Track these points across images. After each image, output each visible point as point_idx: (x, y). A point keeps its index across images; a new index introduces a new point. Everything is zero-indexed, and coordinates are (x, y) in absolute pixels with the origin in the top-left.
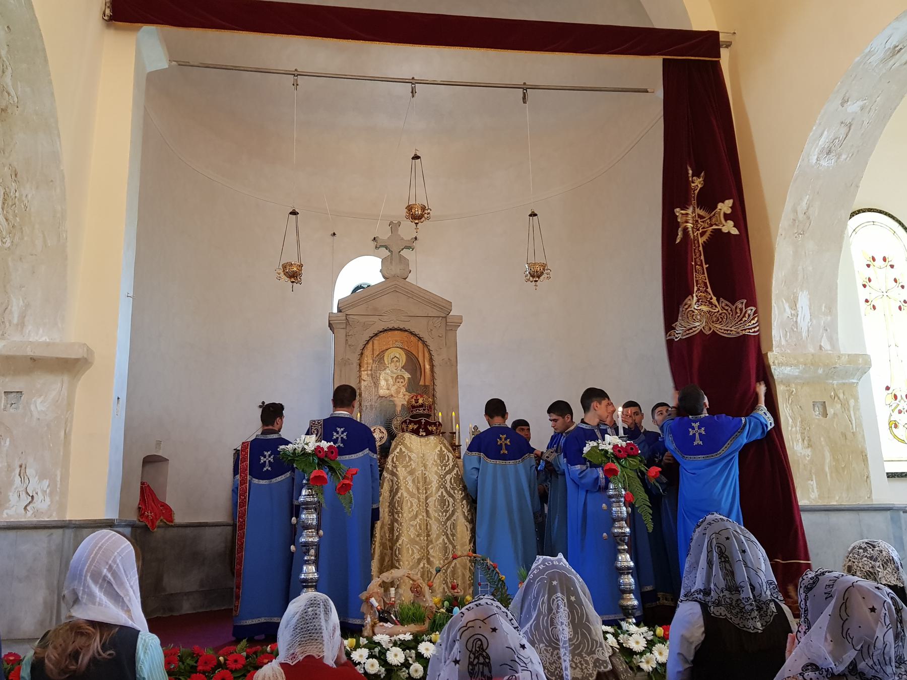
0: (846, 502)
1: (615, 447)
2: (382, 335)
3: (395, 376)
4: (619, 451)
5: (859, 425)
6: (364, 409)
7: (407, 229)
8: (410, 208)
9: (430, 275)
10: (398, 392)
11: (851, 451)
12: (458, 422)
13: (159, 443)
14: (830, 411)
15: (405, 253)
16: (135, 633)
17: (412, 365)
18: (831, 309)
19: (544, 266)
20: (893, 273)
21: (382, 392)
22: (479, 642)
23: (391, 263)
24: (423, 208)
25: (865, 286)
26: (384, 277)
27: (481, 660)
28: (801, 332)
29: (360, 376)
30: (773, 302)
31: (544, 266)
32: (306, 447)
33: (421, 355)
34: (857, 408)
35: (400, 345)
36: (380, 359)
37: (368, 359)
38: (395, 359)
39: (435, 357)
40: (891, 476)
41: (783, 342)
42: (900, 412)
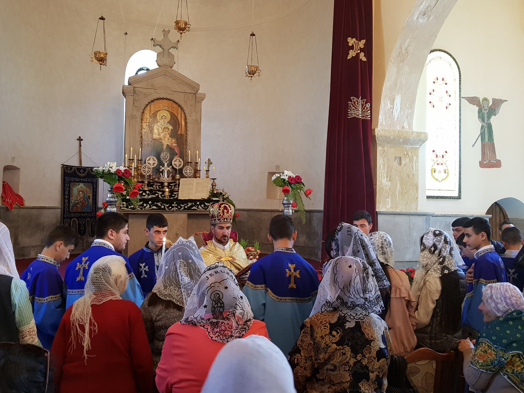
0: (404, 211)
1: (290, 177)
2: (156, 102)
3: (163, 127)
4: (292, 180)
5: (417, 170)
6: (144, 146)
7: (174, 35)
8: (177, 23)
9: (187, 66)
10: (165, 137)
11: (410, 183)
12: (200, 157)
13: (13, 158)
14: (403, 162)
15: (172, 51)
16: (11, 279)
17: (174, 121)
18: (412, 106)
19: (257, 68)
20: (446, 88)
21: (155, 136)
22: (218, 295)
23: (163, 56)
24: (186, 24)
25: (430, 94)
26: (158, 65)
27: (219, 305)
28: (394, 118)
29: (142, 126)
30: (382, 101)
31: (257, 68)
32: (110, 169)
33: (179, 116)
34: (417, 161)
35: (166, 108)
36: (154, 115)
37: (147, 115)
38: (164, 117)
39: (188, 118)
40: (428, 197)
41: (384, 123)
42: (438, 164)
